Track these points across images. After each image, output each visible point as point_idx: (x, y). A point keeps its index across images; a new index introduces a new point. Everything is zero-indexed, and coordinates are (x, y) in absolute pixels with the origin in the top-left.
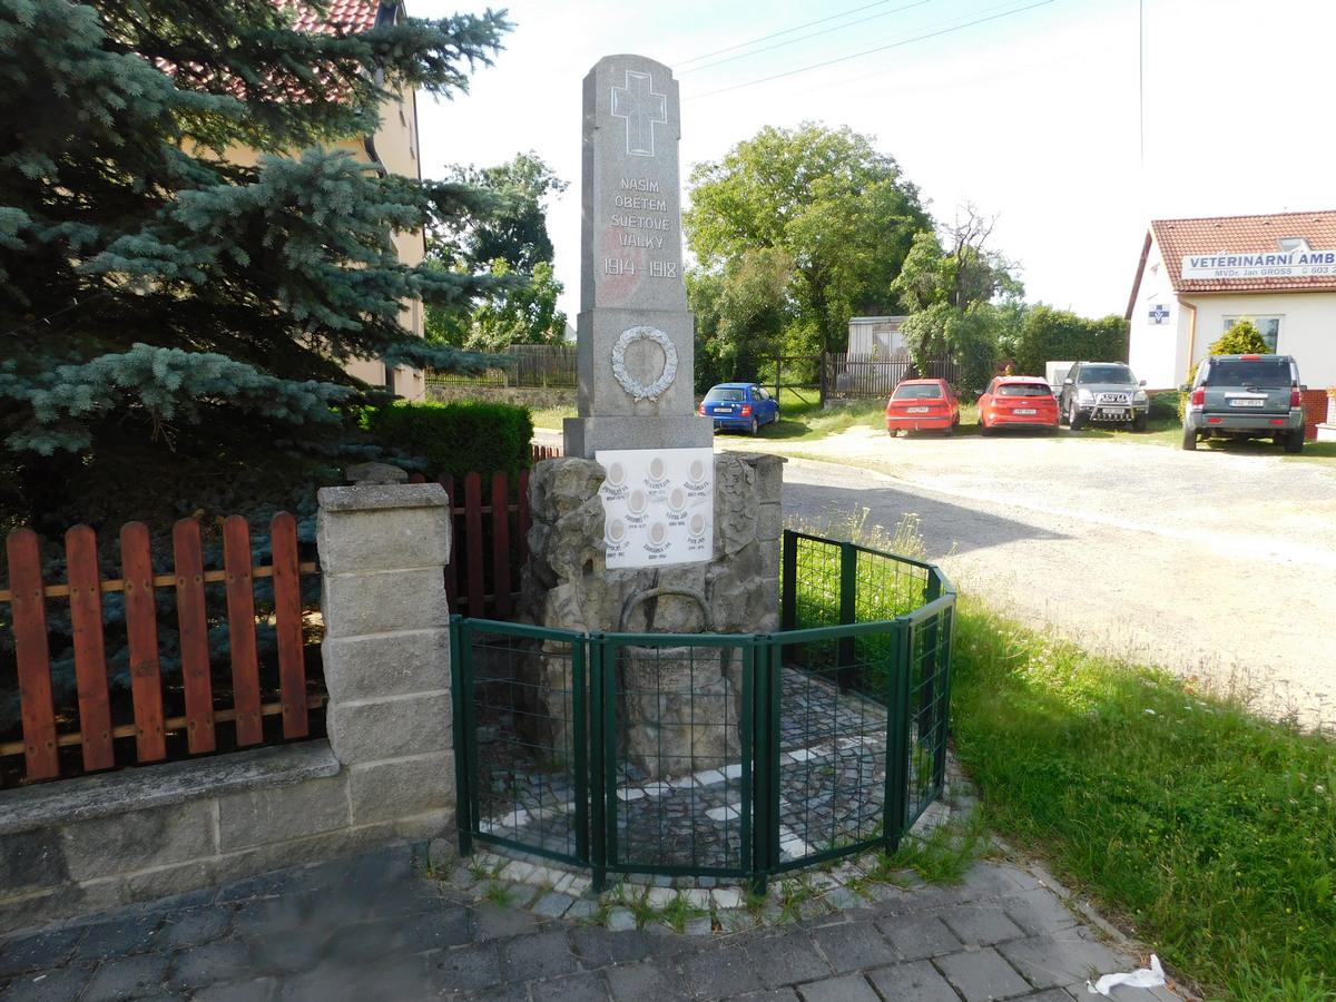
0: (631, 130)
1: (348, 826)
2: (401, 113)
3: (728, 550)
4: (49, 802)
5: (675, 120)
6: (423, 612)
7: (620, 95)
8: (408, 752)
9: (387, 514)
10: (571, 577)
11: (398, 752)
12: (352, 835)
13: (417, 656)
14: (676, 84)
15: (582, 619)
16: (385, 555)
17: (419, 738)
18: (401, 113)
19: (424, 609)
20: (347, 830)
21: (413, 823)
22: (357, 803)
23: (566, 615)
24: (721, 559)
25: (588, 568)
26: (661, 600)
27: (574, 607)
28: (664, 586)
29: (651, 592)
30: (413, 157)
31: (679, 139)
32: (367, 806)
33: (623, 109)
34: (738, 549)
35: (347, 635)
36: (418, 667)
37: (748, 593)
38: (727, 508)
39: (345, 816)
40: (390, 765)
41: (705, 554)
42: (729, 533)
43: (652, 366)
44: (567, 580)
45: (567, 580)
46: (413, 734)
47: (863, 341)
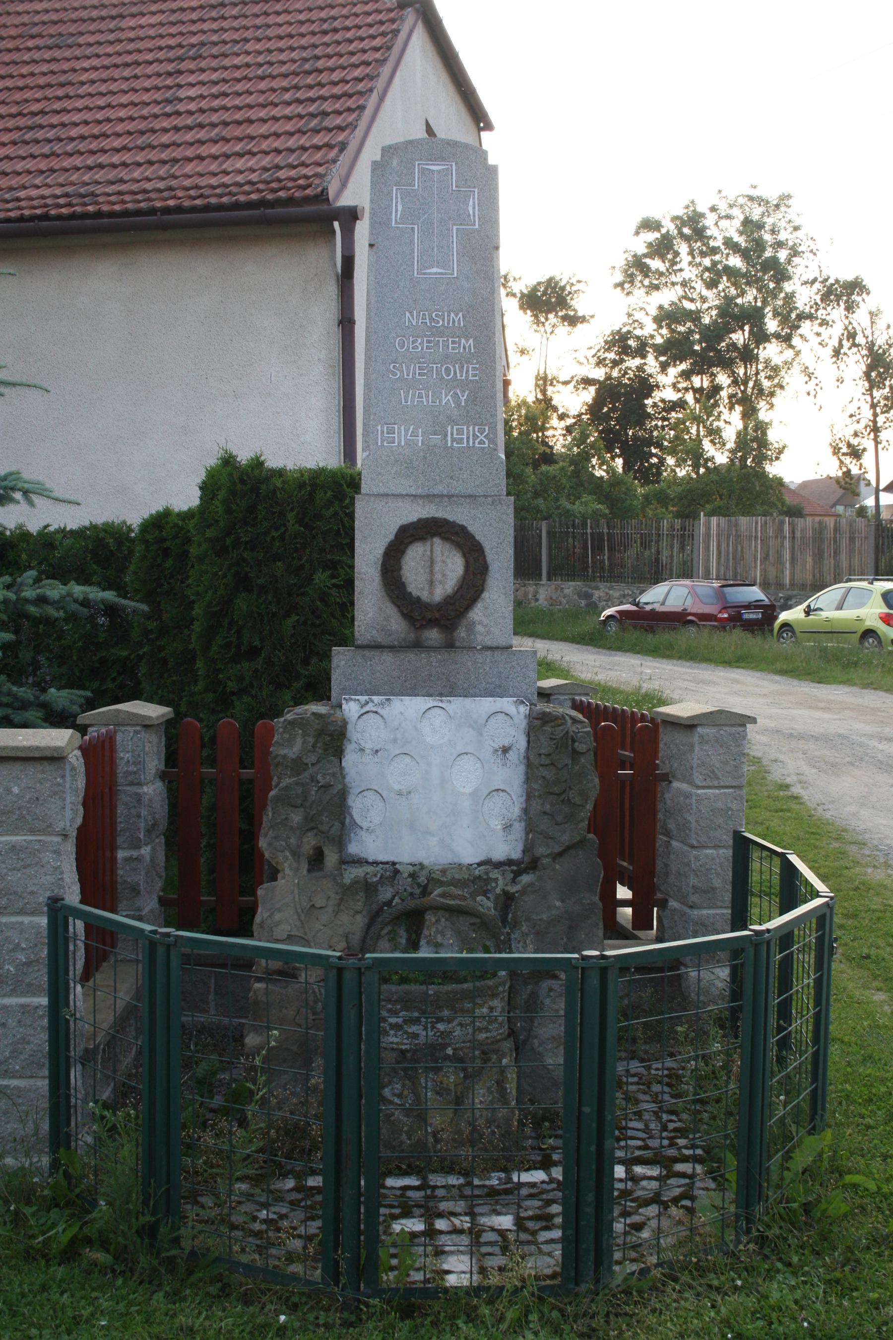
6: (32, 893)
13: (24, 949)
17: (22, 1057)
19: (34, 889)
25: (317, 860)
26: (430, 917)
29: (412, 904)
34: (558, 849)
43: (444, 575)
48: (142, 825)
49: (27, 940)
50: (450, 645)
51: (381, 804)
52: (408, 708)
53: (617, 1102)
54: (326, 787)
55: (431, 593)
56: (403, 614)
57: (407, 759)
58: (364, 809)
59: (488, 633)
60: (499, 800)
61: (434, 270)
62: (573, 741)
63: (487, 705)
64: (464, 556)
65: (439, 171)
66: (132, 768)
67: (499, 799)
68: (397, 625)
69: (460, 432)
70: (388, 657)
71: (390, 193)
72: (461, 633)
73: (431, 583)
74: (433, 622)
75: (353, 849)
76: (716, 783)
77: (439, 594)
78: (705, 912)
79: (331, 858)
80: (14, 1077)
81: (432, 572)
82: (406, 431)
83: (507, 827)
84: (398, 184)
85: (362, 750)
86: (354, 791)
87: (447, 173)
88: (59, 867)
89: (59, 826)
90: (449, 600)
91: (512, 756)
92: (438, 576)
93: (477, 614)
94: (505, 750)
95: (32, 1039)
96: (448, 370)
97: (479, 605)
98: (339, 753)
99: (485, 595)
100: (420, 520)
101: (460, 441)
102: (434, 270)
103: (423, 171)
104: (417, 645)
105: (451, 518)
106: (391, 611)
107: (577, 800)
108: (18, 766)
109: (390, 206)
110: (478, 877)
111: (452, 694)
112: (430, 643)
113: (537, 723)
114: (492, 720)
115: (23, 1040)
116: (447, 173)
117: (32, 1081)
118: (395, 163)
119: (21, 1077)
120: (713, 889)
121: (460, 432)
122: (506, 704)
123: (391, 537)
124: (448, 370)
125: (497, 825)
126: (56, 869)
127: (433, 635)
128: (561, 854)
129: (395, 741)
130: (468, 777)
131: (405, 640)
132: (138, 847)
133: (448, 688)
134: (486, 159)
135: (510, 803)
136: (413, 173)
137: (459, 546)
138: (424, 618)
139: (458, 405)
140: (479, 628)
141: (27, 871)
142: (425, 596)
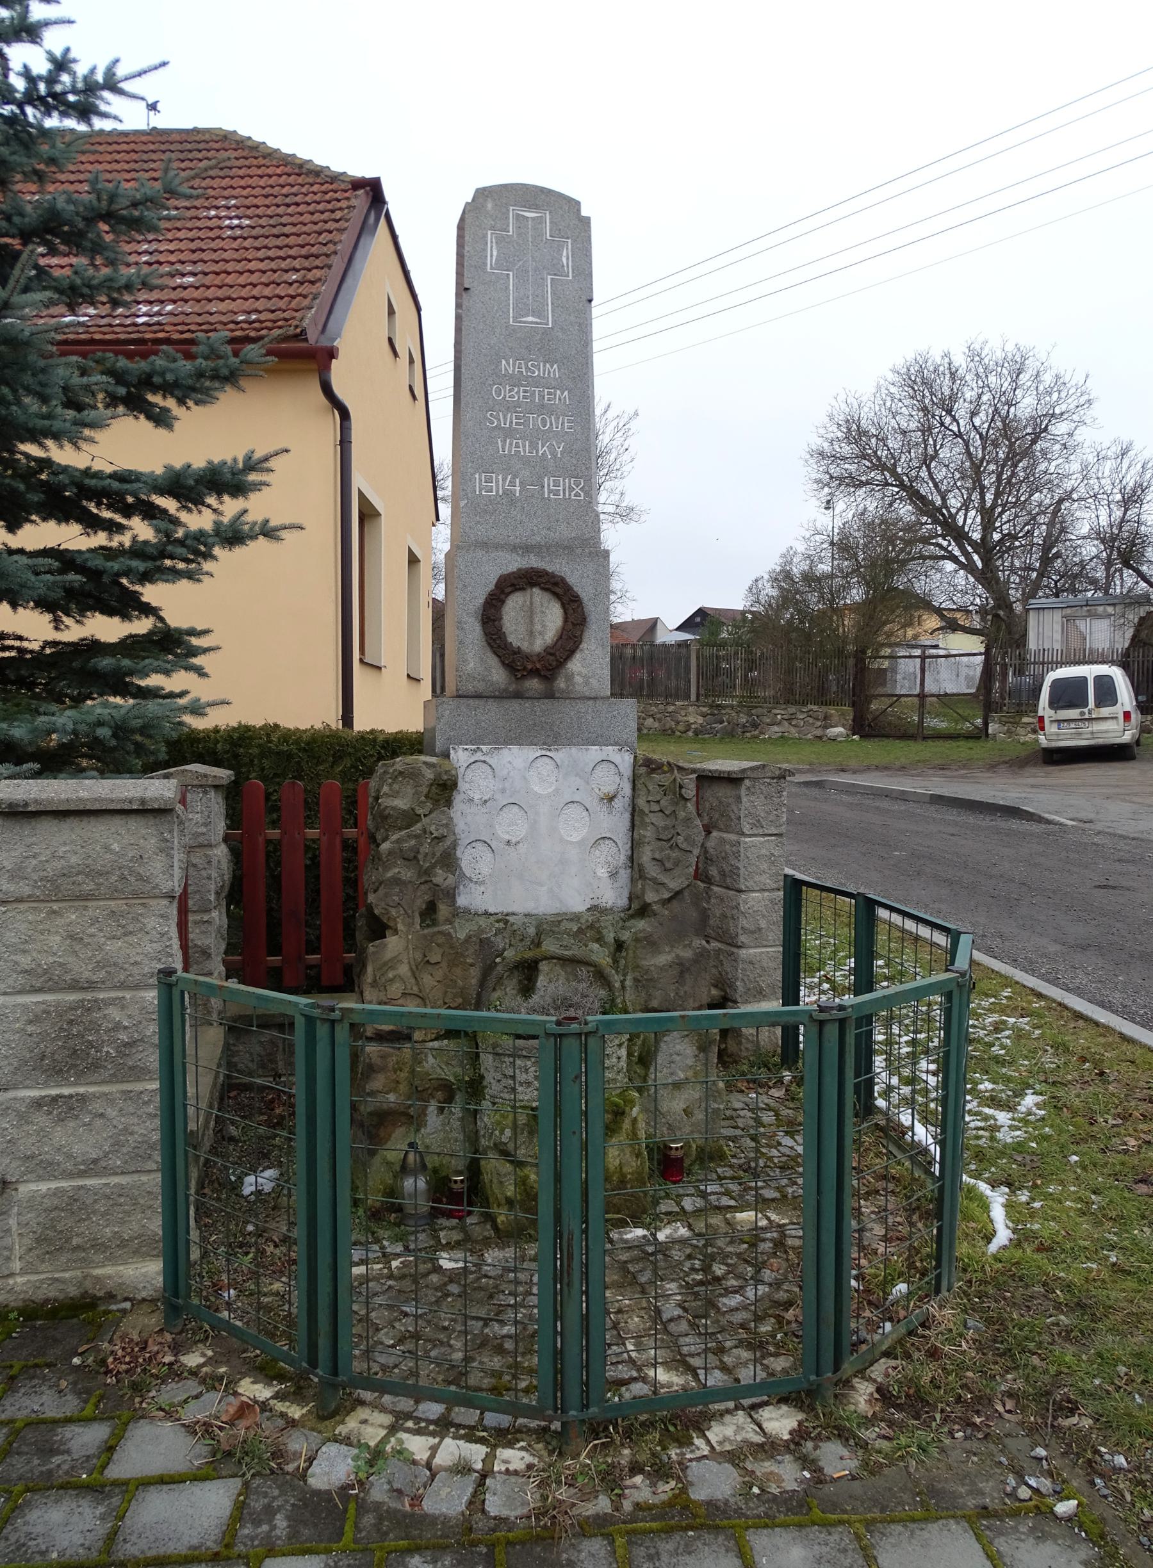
0: (516, 288)
1: (11, 1275)
2: (390, 341)
3: (651, 897)
4: (93, 1167)
5: (584, 272)
6: (136, 963)
7: (500, 240)
8: (106, 1172)
9: (86, 819)
10: (400, 927)
11: (93, 1167)
12: (18, 1289)
13: (126, 1028)
14: (586, 221)
15: (415, 990)
16: (80, 878)
17: (125, 1150)
18: (390, 341)
19: (138, 959)
20: (11, 1282)
21: (110, 1277)
22: (27, 1241)
23: (392, 980)
24: (639, 909)
25: (429, 912)
26: (544, 966)
27: (404, 969)
28: (550, 946)
29: (529, 955)
30: (414, 397)
31: (590, 301)
32: (51, 1242)
33: (504, 262)
34: (667, 896)
35: (20, 992)
36: (126, 1045)
37: (681, 964)
38: (648, 833)
39: (8, 1259)
40: (81, 1187)
41: (613, 896)
42: (652, 870)
43: (544, 626)
44: (396, 932)
45: (396, 932)
46: (117, 1143)
47: (1048, 633)
48: (213, 887)
49: (129, 1016)
50: (550, 695)
51: (490, 855)
52: (515, 759)
53: (250, 1179)
54: (440, 839)
55: (531, 644)
56: (503, 663)
57: (515, 809)
58: (473, 860)
59: (587, 683)
60: (606, 848)
61: (530, 319)
62: (681, 787)
63: (594, 753)
64: (563, 606)
65: (533, 219)
66: (203, 829)
67: (606, 847)
68: (499, 676)
69: (556, 484)
70: (493, 706)
71: (485, 236)
72: (561, 683)
73: (531, 633)
74: (535, 673)
75: (462, 901)
76: (760, 831)
77: (538, 646)
78: (752, 951)
79: (443, 910)
80: (116, 1174)
81: (532, 623)
82: (504, 480)
83: (613, 875)
84: (493, 228)
85: (471, 800)
86: (463, 842)
87: (540, 221)
88: (167, 933)
89: (166, 886)
90: (549, 651)
91: (618, 803)
92: (538, 627)
93: (575, 665)
94: (611, 799)
95: (136, 1128)
96: (544, 421)
97: (578, 655)
98: (449, 803)
99: (584, 645)
100: (519, 570)
101: (556, 493)
102: (530, 319)
103: (518, 217)
104: (518, 695)
105: (549, 568)
106: (493, 660)
107: (684, 846)
108: (118, 821)
109: (485, 250)
110: (589, 925)
111: (555, 743)
112: (531, 694)
113: (643, 770)
114: (598, 769)
115: (126, 1131)
116: (540, 221)
117: (136, 1177)
118: (489, 206)
119: (123, 1173)
120: (760, 929)
121: (556, 484)
122: (610, 752)
123: (492, 586)
124: (544, 421)
125: (602, 872)
126: (163, 935)
127: (534, 684)
128: (670, 900)
129: (503, 791)
130: (576, 828)
131: (505, 690)
132: (208, 911)
133: (550, 738)
134: (579, 210)
135: (615, 850)
136: (507, 218)
137: (557, 596)
138: (525, 669)
139: (554, 455)
140: (578, 679)
141: (130, 939)
142: (525, 647)
